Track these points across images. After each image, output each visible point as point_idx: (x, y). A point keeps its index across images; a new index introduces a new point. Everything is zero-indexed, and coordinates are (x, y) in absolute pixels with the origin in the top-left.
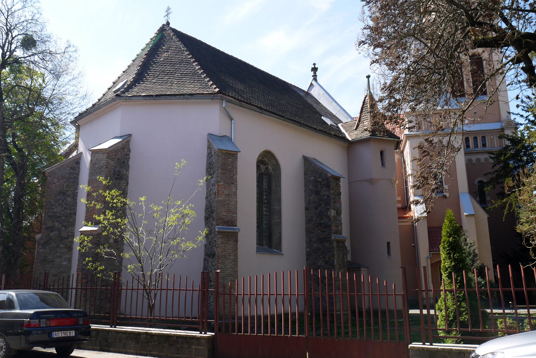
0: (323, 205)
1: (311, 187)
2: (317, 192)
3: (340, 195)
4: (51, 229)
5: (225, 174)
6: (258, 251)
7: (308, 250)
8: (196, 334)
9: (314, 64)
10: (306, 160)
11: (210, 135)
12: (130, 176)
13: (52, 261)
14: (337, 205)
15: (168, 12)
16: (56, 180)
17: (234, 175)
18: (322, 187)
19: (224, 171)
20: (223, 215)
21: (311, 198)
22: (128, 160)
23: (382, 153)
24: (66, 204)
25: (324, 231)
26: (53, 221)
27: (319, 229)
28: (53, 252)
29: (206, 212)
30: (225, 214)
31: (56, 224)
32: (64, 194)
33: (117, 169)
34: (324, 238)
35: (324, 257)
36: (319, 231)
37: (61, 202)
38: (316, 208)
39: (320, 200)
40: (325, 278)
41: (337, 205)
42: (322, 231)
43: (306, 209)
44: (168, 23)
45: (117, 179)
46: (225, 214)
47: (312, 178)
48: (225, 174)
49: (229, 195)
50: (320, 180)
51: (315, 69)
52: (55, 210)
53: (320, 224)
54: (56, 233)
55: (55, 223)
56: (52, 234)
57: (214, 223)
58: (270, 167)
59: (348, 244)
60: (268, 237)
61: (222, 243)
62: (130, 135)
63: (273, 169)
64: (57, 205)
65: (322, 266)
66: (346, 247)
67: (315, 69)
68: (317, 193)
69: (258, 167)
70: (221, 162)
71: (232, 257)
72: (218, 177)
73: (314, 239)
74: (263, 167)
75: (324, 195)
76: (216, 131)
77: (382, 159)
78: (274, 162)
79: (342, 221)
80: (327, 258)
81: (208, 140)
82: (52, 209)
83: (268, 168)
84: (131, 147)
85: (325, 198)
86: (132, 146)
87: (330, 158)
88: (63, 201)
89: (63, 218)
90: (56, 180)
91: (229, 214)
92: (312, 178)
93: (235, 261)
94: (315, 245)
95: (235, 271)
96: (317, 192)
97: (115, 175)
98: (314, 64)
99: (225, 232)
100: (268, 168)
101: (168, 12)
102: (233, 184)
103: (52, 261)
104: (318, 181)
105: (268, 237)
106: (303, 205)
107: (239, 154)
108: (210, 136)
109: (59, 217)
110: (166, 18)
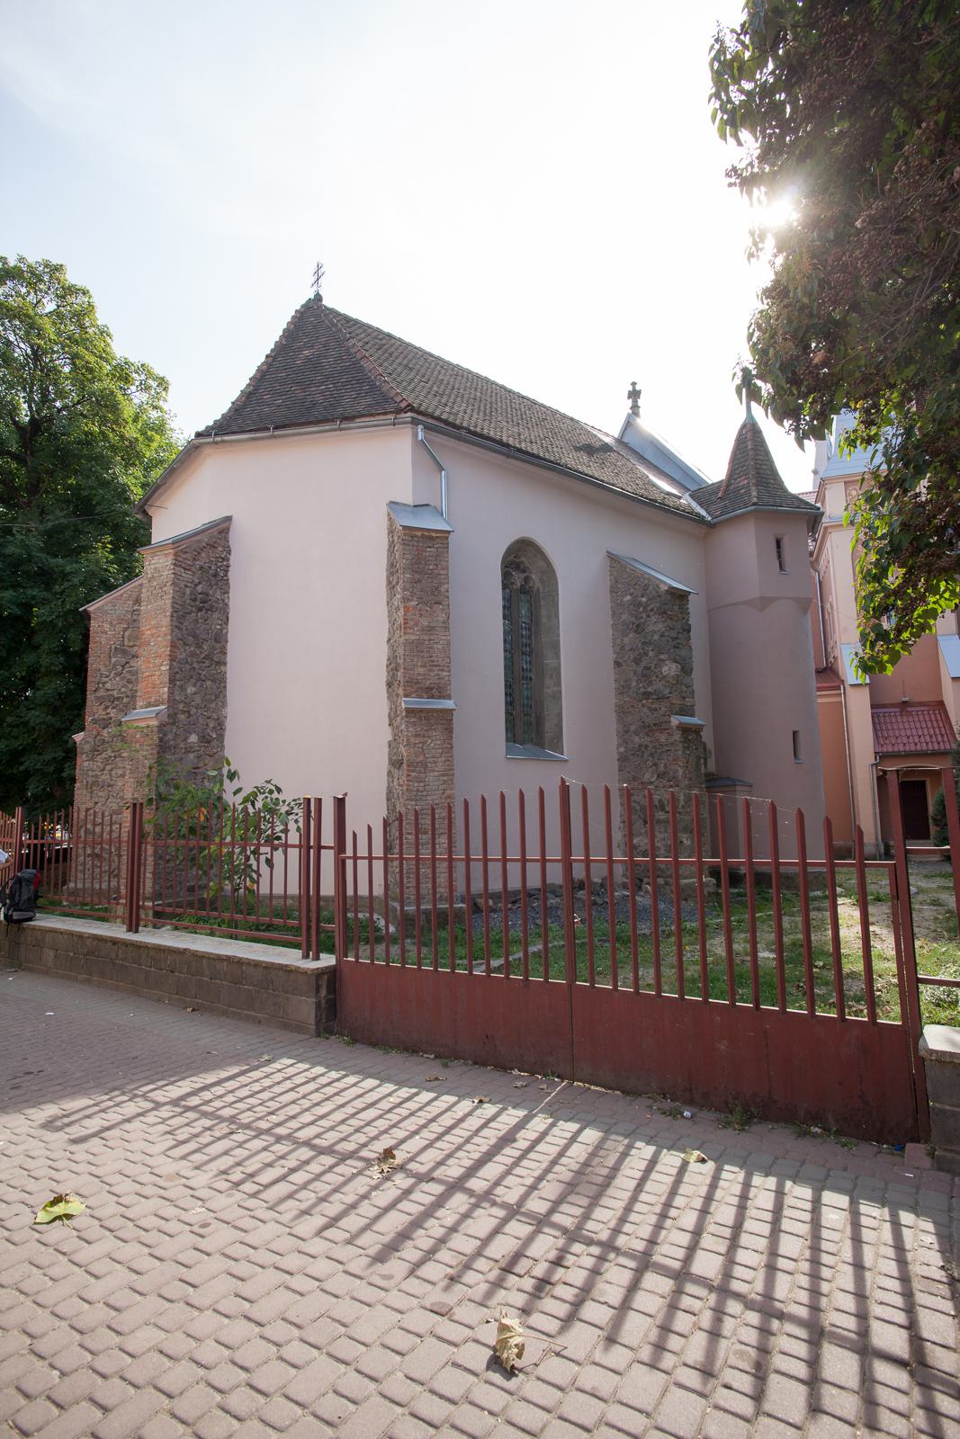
0: (651, 654)
1: (624, 617)
2: (638, 626)
3: (689, 631)
4: (106, 723)
5: (419, 581)
6: (508, 751)
7: (622, 749)
8: (291, 957)
9: (634, 384)
10: (612, 558)
11: (392, 503)
12: (232, 604)
13: (109, 786)
14: (683, 652)
15: (318, 274)
16: (106, 627)
17: (441, 584)
18: (648, 616)
19: (417, 576)
20: (419, 674)
21: (626, 640)
22: (227, 571)
23: (778, 543)
24: (130, 672)
25: (656, 710)
26: (107, 708)
27: (643, 706)
28: (108, 767)
29: (388, 672)
30: (421, 670)
31: (113, 713)
32: (124, 652)
33: (199, 588)
34: (655, 725)
35: (655, 764)
36: (645, 710)
37: (120, 668)
38: (637, 661)
39: (644, 643)
40: (143, 836)
41: (683, 652)
42: (650, 709)
43: (617, 664)
44: (318, 298)
45: (200, 610)
46: (421, 670)
47: (628, 598)
48: (419, 581)
49: (431, 629)
50: (644, 600)
51: (634, 394)
52: (108, 686)
53: (647, 695)
54: (112, 730)
55: (109, 710)
56: (105, 733)
57: (401, 692)
58: (533, 576)
59: (707, 736)
60: (529, 721)
61: (417, 736)
62: (229, 519)
63: (541, 581)
64: (112, 675)
65: (652, 783)
66: (705, 744)
67: (634, 394)
68: (639, 629)
69: (506, 576)
70: (420, 559)
71: (440, 767)
72: (404, 589)
73: (633, 728)
74: (518, 579)
75: (654, 632)
76: (407, 497)
77: (779, 556)
78: (542, 563)
79: (695, 687)
80: (661, 768)
81: (389, 515)
82: (104, 683)
83: (524, 572)
84: (231, 543)
85: (656, 637)
86: (235, 540)
87: (667, 566)
88: (123, 666)
89: (125, 700)
90: (106, 627)
91: (431, 670)
92: (628, 598)
93: (447, 775)
94: (637, 739)
95: (448, 797)
96: (638, 626)
97: (195, 600)
98: (634, 384)
99: (421, 711)
100: (524, 572)
101: (318, 274)
102: (440, 603)
103: (109, 786)
104: (640, 604)
105: (529, 721)
106: (611, 657)
107: (451, 537)
108: (392, 505)
109: (118, 698)
110: (315, 287)
